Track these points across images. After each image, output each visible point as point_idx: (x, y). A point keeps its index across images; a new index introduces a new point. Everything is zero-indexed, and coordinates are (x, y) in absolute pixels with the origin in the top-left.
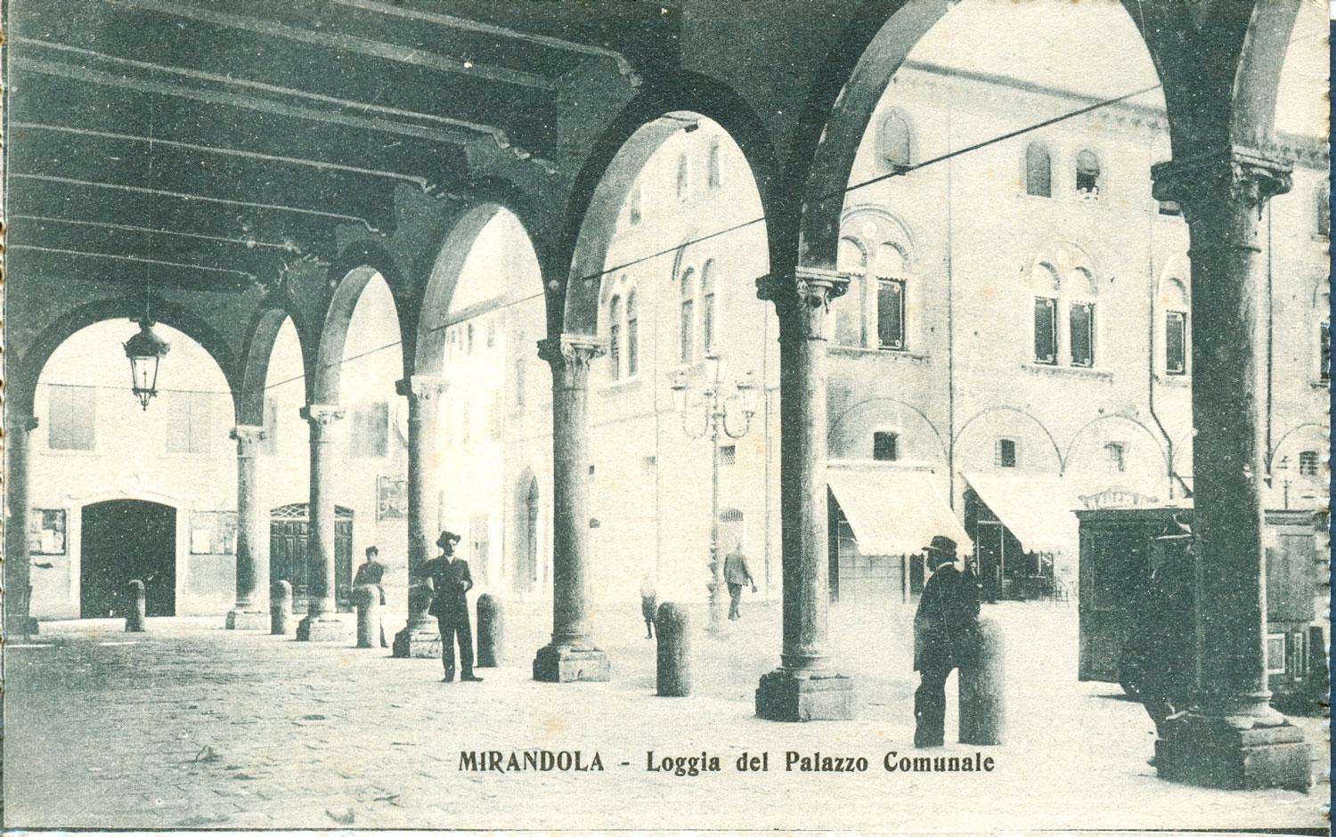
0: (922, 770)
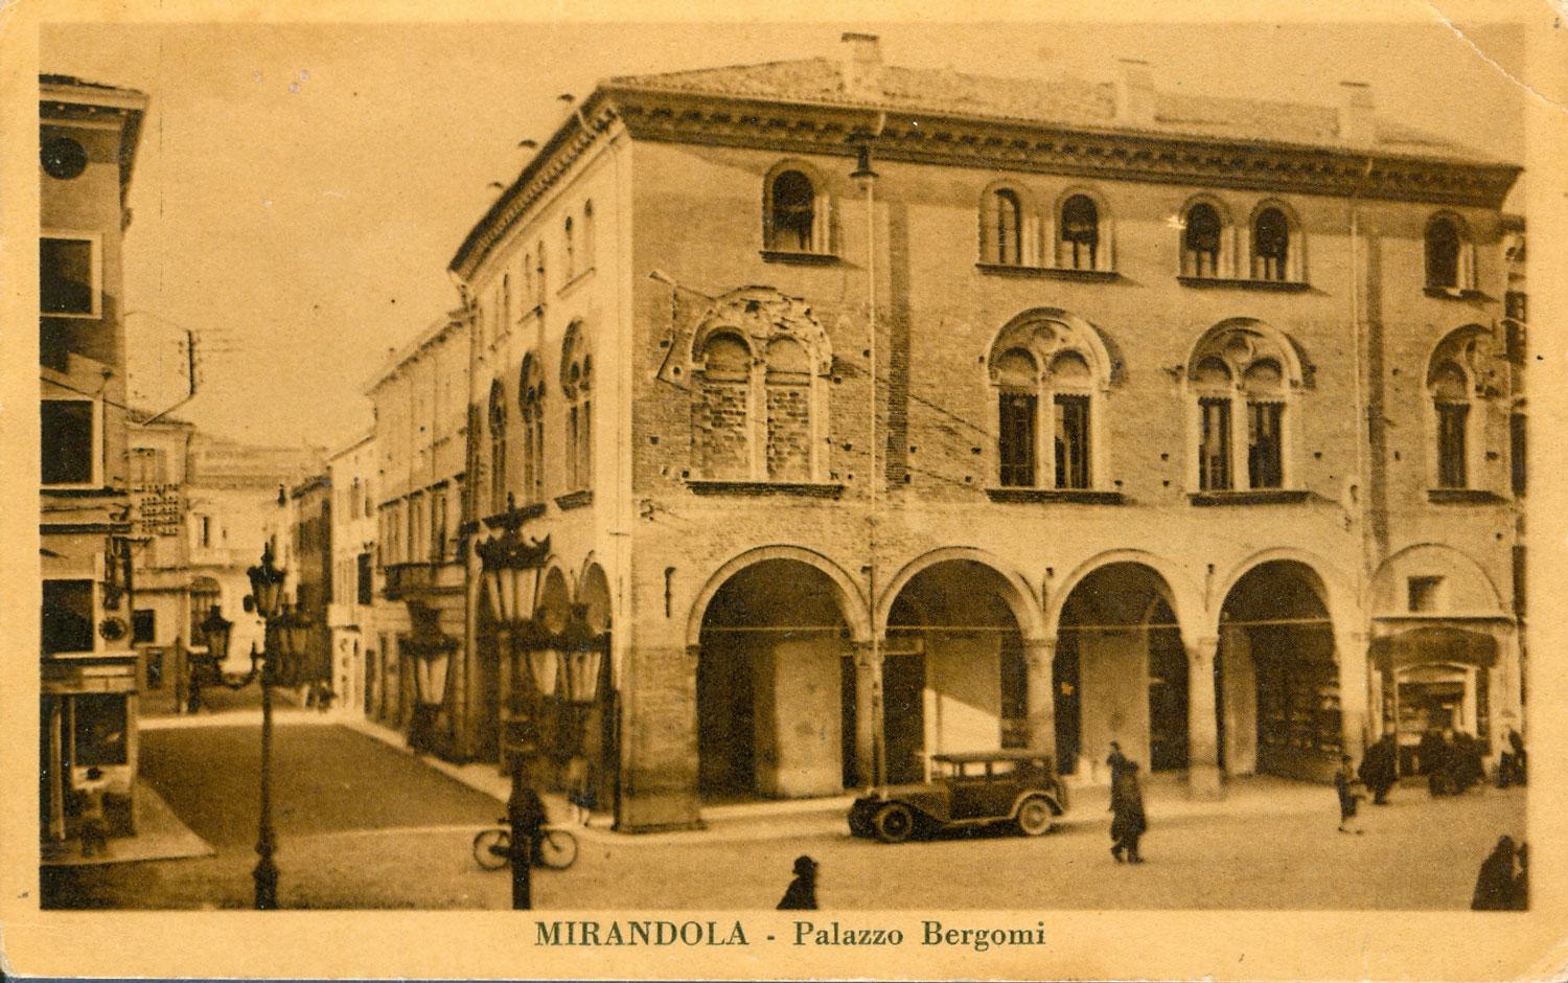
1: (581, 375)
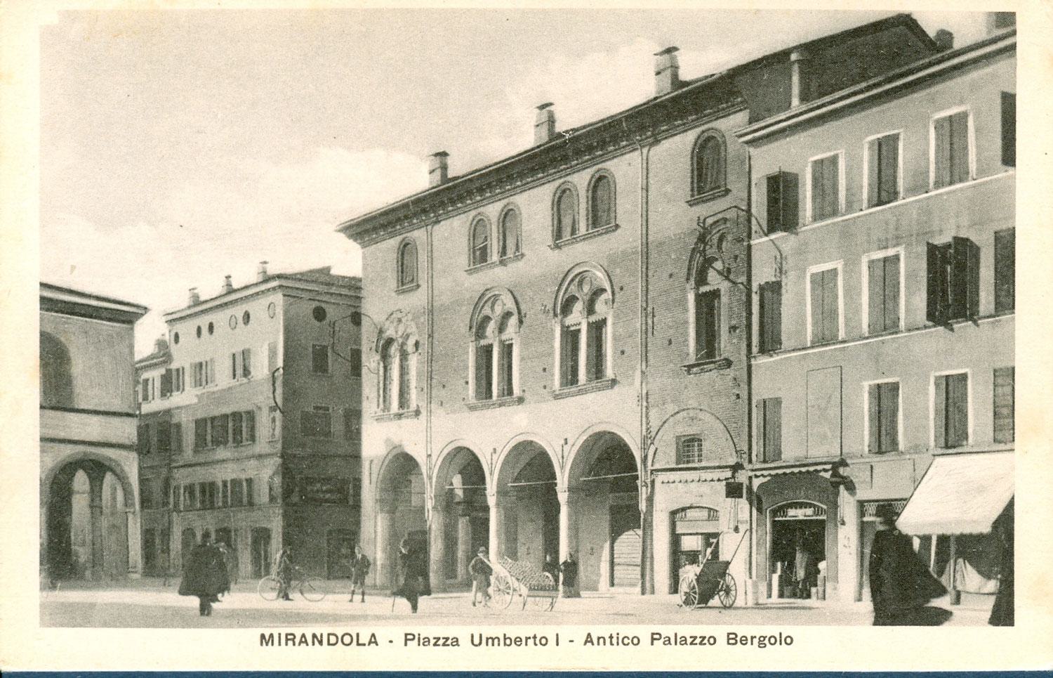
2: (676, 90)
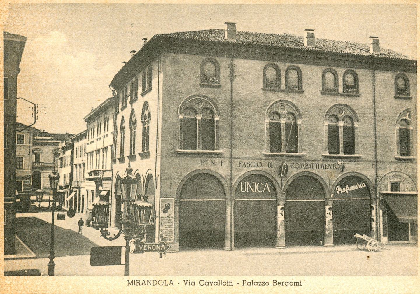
0: (297, 285)
1: (147, 118)
2: (28, 251)
